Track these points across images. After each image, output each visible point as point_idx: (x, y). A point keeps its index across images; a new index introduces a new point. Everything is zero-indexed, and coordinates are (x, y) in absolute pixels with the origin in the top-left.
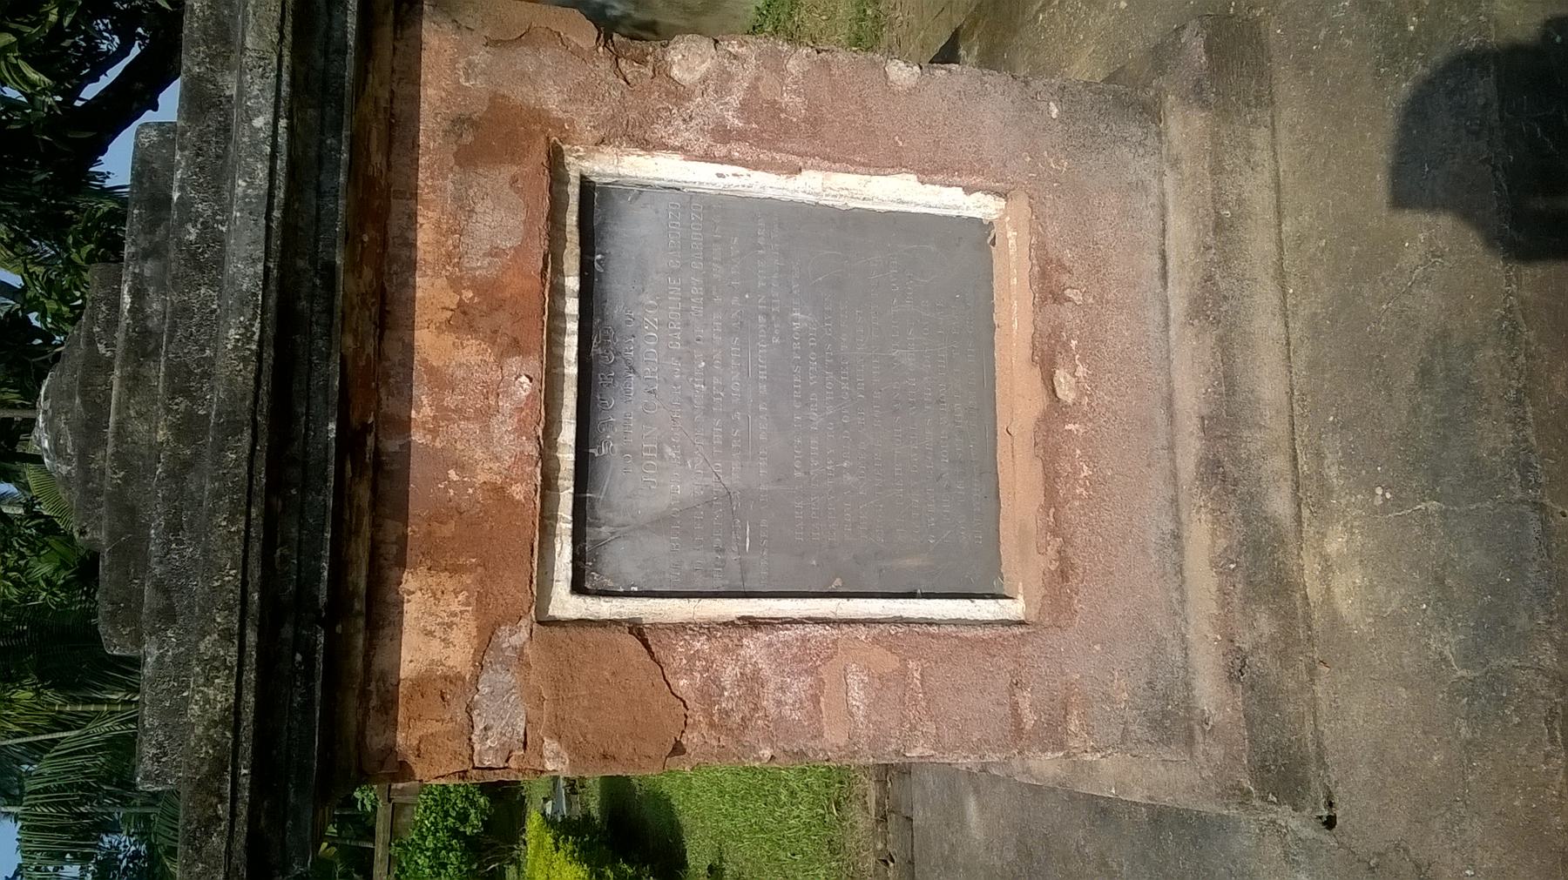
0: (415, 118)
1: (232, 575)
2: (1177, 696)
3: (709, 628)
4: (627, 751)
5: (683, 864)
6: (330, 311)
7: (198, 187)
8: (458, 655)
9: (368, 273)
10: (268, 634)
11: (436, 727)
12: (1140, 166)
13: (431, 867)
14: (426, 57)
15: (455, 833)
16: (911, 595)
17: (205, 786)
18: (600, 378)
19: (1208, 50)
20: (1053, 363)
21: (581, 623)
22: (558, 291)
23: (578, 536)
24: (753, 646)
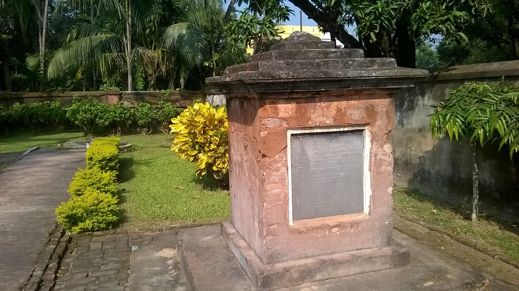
1: (302, 76)
6: (342, 88)
8: (281, 114)
11: (269, 112)
12: (378, 242)
13: (85, 109)
15: (96, 116)
18: (321, 136)
19: (403, 253)
20: (339, 227)
22: (345, 127)
23: (309, 134)
24: (284, 169)
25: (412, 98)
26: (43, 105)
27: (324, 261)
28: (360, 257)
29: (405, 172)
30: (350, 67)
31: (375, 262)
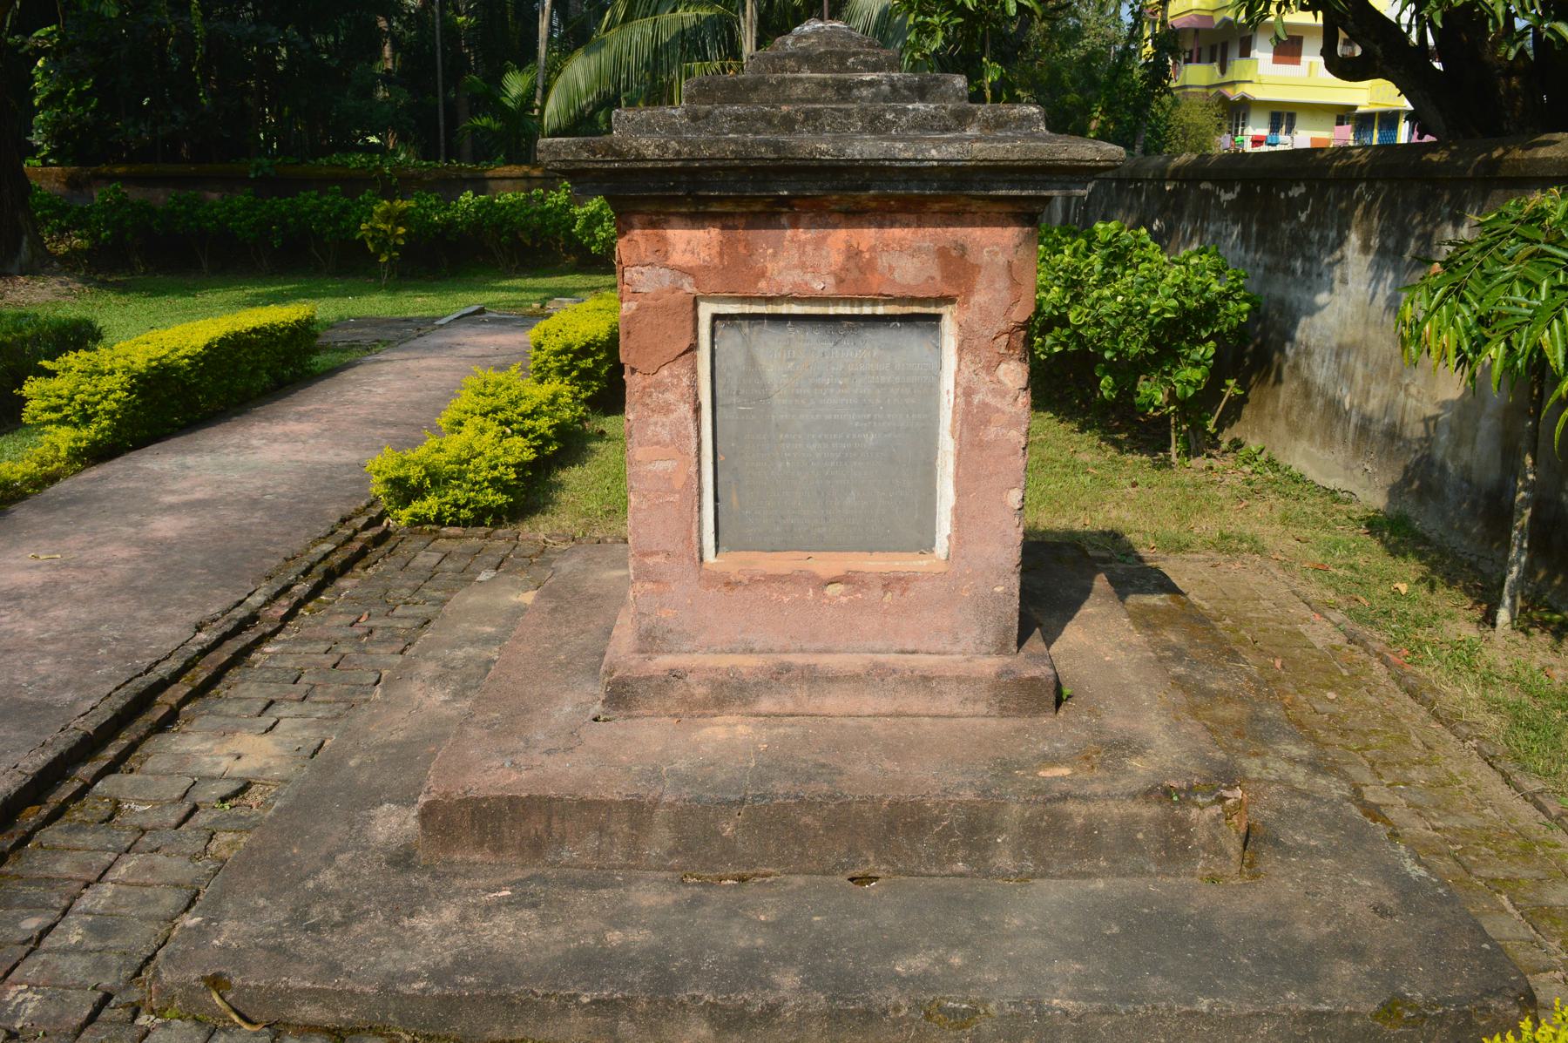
0: (962, 225)
1: (707, 153)
3: (694, 386)
4: (631, 344)
5: (607, 414)
8: (678, 257)
9: (874, 204)
10: (680, 170)
11: (643, 248)
12: (969, 639)
14: (998, 230)
16: (716, 499)
17: (610, 149)
18: (830, 326)
19: (1033, 679)
21: (696, 319)
22: (874, 302)
23: (743, 316)
24: (685, 410)
25: (1429, 227)
26: (529, 199)
27: (788, 668)
28: (894, 671)
29: (1384, 460)
30: (888, 129)
31: (940, 693)
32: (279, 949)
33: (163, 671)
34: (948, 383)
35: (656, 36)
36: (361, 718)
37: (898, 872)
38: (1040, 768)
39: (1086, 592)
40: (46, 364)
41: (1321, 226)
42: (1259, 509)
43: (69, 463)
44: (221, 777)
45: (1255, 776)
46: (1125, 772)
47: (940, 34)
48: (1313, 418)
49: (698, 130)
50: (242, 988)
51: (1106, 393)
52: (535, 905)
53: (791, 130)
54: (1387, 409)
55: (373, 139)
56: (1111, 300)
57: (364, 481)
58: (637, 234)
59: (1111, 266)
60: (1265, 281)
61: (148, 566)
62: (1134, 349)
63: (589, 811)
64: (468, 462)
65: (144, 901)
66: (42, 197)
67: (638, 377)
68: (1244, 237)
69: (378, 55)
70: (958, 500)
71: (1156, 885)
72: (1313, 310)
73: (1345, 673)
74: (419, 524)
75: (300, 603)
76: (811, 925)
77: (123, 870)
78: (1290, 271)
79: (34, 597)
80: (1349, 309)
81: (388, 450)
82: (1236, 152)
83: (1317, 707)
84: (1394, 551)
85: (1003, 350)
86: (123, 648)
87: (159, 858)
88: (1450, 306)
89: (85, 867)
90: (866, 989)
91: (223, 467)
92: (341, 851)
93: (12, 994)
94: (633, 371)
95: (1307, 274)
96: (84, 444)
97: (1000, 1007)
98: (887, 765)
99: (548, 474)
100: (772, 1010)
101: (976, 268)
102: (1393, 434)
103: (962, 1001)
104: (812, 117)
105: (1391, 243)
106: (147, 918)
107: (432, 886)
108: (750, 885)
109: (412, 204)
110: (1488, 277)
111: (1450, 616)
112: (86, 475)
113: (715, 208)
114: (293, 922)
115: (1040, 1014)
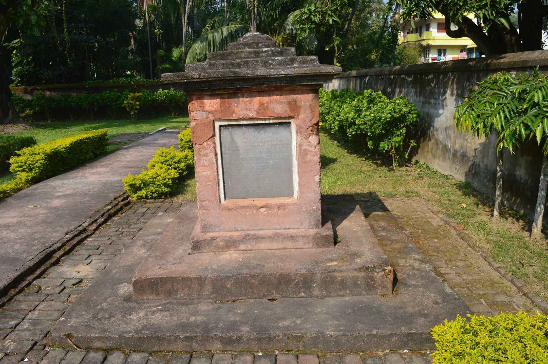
0: (295, 94)
2: (210, 230)
3: (215, 147)
7: (278, 62)
8: (207, 108)
9: (267, 89)
11: (196, 105)
12: (306, 224)
14: (306, 95)
16: (224, 183)
18: (249, 128)
19: (326, 235)
21: (214, 127)
22: (269, 119)
23: (229, 125)
24: (212, 155)
30: (270, 66)
32: (88, 326)
33: (55, 247)
34: (294, 143)
35: (222, 34)
36: (117, 258)
37: (283, 297)
38: (327, 262)
39: (352, 210)
40: (17, 152)
41: (438, 88)
42: (421, 182)
43: (26, 184)
44: (73, 278)
45: (402, 265)
46: (354, 263)
47: (307, 31)
48: (439, 152)
49: (212, 69)
50: (77, 337)
51: (370, 147)
52: (168, 311)
53: (240, 67)
54: (461, 147)
55: (128, 73)
56: (368, 115)
57: (122, 186)
58: (194, 102)
59: (369, 104)
60: (423, 107)
61: (51, 215)
62: (377, 132)
63: (185, 281)
64: (156, 178)
65: (48, 315)
66: (16, 97)
67: (197, 146)
68: (416, 93)
69: (129, 44)
70: (299, 180)
71: (365, 298)
72: (438, 115)
73: (442, 233)
74: (140, 199)
75: (100, 225)
76: (254, 313)
77: (41, 306)
78: (429, 103)
79: (14, 226)
80: (448, 115)
81: (129, 175)
82: (427, 63)
83: (431, 244)
84: (465, 194)
85: (310, 132)
86: (42, 240)
87: (53, 303)
88: (469, 112)
89: (30, 306)
90: (269, 331)
91: (76, 183)
92: (109, 297)
93: (6, 343)
94: (196, 144)
95: (435, 104)
96: (30, 178)
97: (311, 335)
98: (279, 263)
99: (184, 182)
100: (239, 338)
101: (300, 107)
102: (464, 155)
103: (299, 333)
104: (246, 63)
105: (460, 92)
106: (49, 320)
107: (137, 306)
108: (236, 302)
109: (141, 94)
110: (480, 102)
111: (479, 214)
112: (30, 188)
113: (218, 92)
114: (93, 318)
115: (323, 337)
